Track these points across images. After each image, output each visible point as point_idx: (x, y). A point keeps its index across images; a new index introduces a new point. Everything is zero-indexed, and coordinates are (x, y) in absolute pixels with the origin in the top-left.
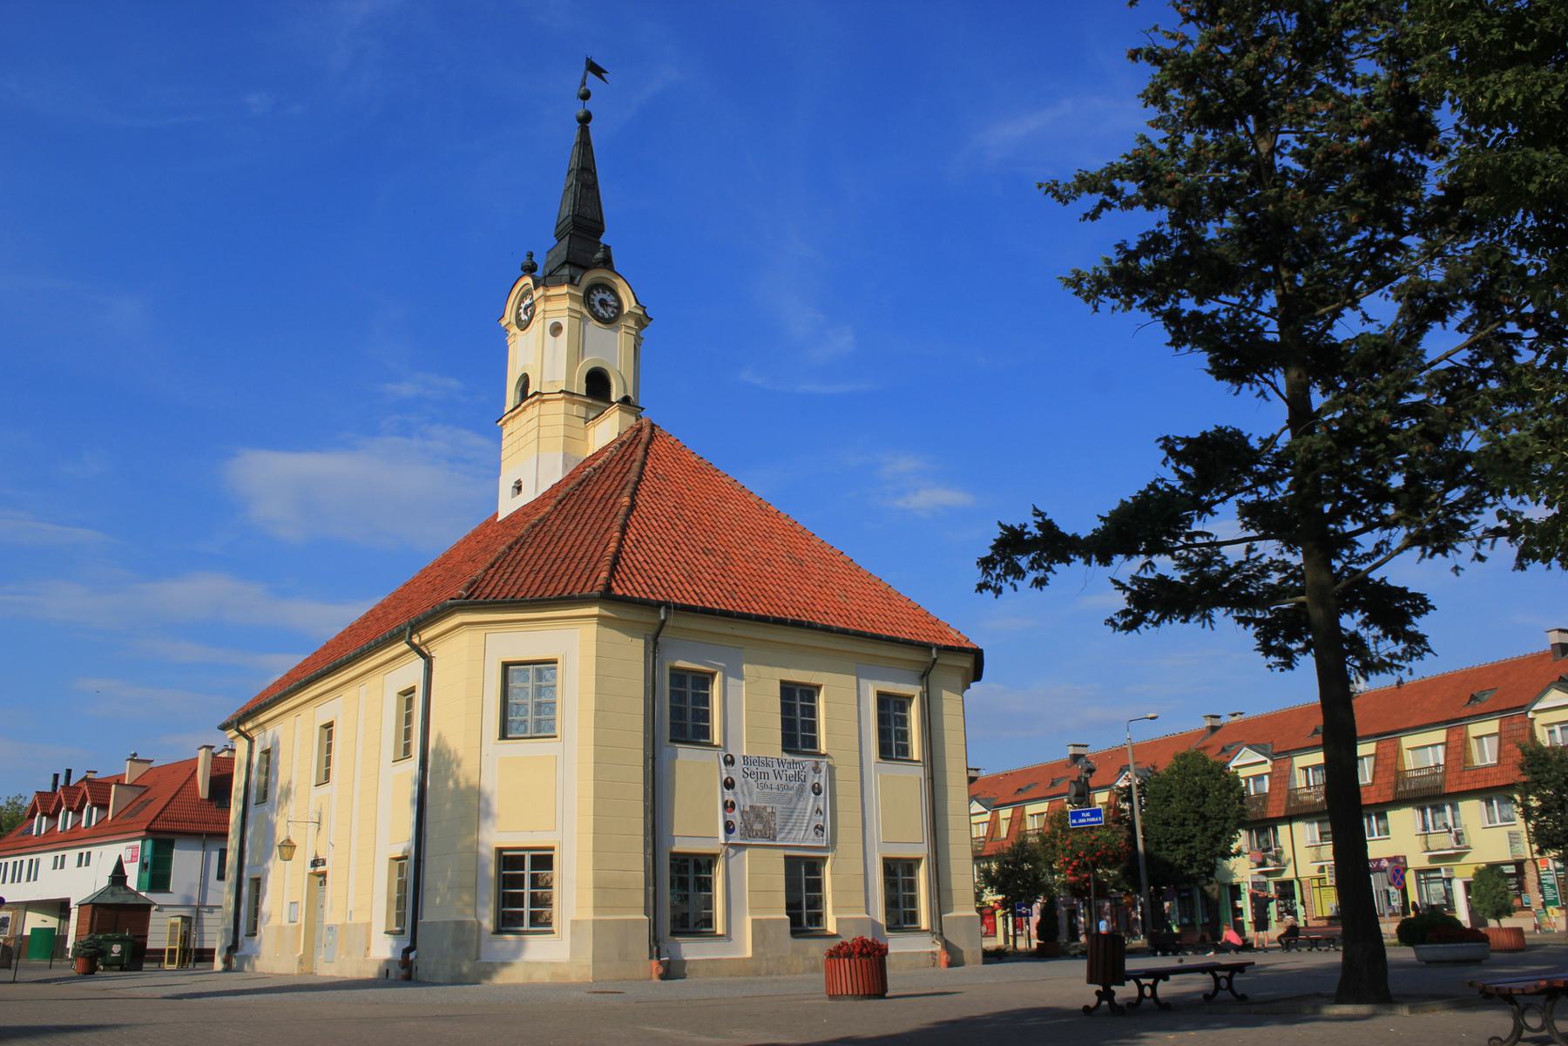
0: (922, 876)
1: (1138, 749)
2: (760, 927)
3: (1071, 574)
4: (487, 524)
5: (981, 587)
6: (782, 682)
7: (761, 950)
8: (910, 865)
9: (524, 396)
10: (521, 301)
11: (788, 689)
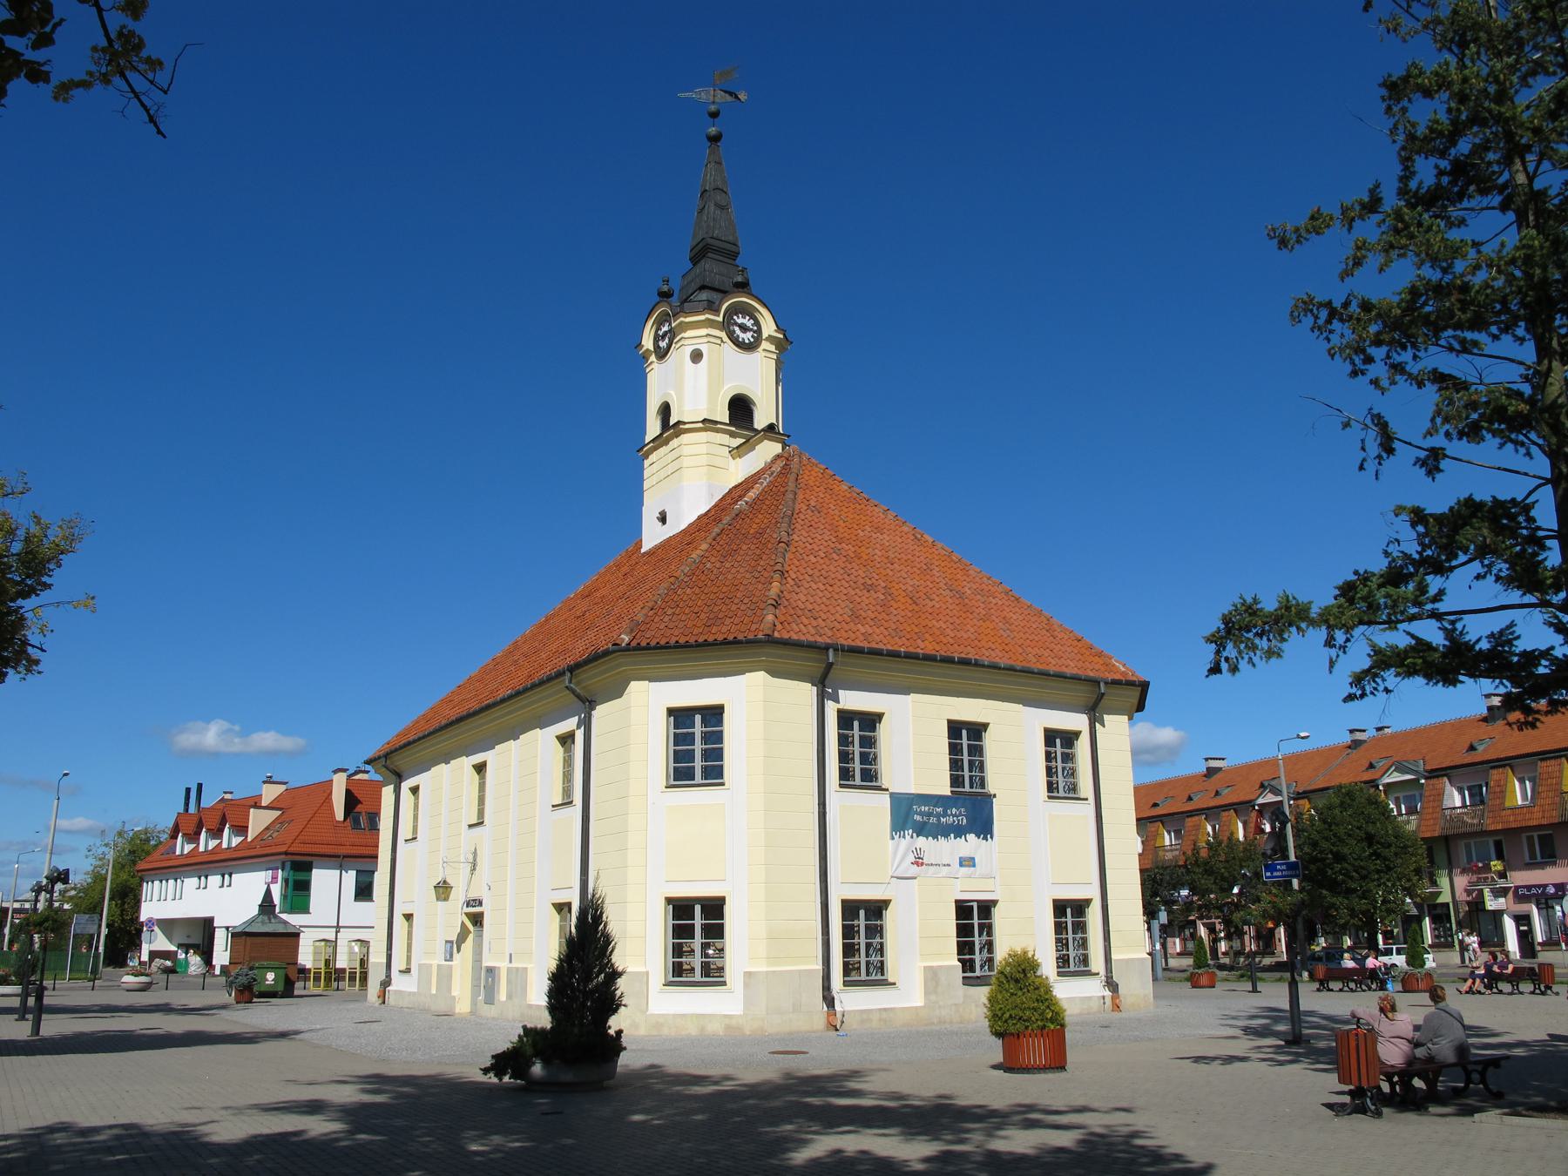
0: (1093, 916)
1: (1293, 760)
2: (932, 975)
3: (1305, 645)
4: (630, 555)
5: (1215, 670)
6: (949, 722)
7: (933, 998)
8: (1080, 907)
9: (665, 425)
10: (658, 329)
11: (955, 728)
